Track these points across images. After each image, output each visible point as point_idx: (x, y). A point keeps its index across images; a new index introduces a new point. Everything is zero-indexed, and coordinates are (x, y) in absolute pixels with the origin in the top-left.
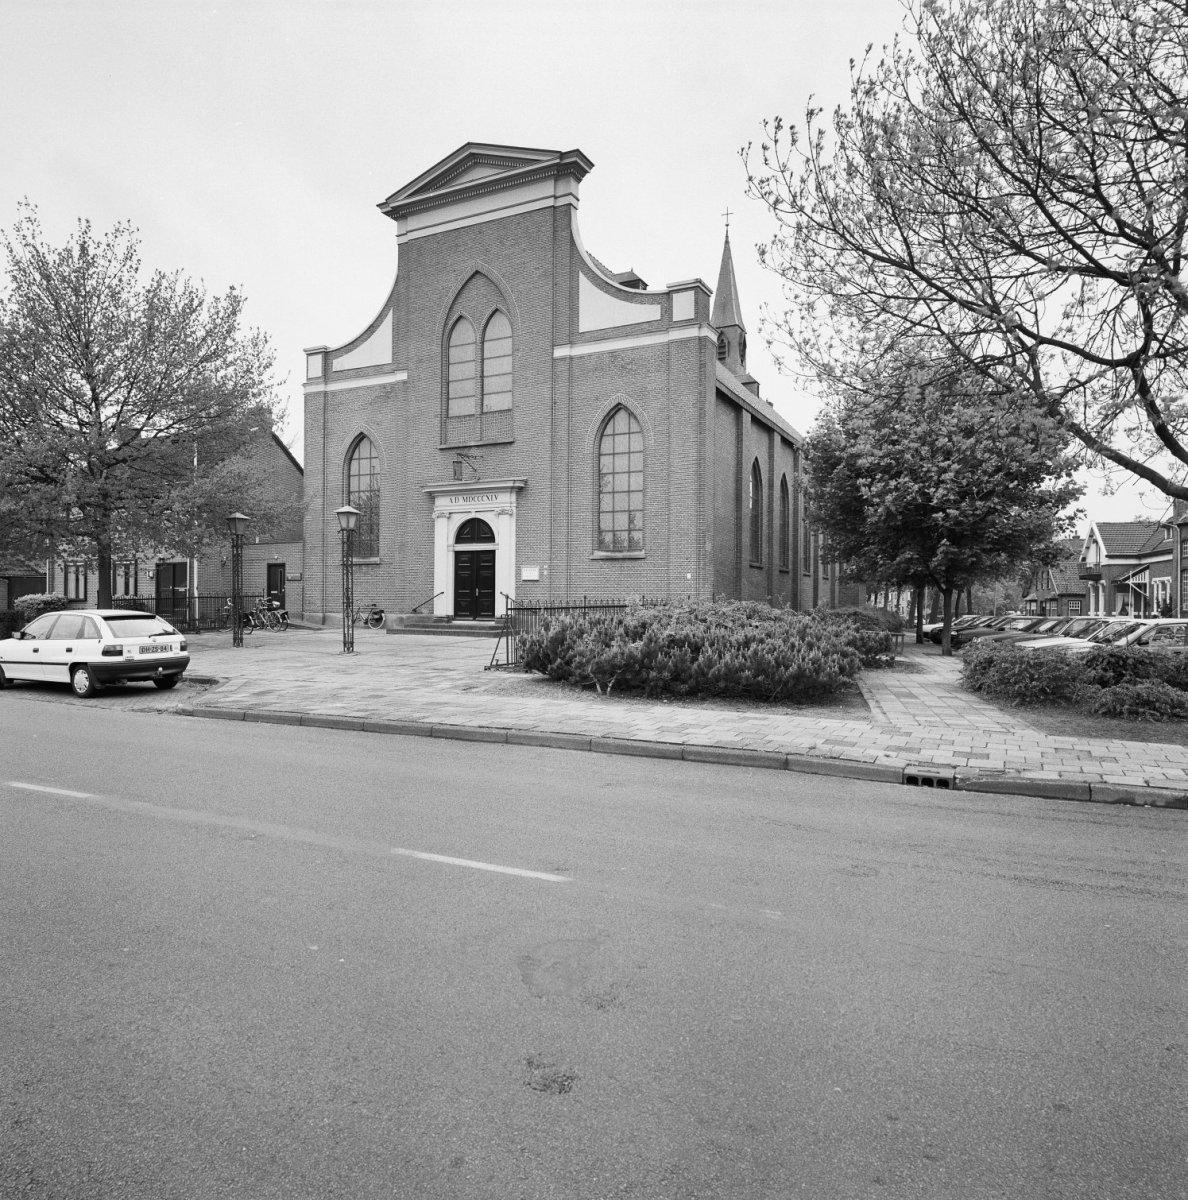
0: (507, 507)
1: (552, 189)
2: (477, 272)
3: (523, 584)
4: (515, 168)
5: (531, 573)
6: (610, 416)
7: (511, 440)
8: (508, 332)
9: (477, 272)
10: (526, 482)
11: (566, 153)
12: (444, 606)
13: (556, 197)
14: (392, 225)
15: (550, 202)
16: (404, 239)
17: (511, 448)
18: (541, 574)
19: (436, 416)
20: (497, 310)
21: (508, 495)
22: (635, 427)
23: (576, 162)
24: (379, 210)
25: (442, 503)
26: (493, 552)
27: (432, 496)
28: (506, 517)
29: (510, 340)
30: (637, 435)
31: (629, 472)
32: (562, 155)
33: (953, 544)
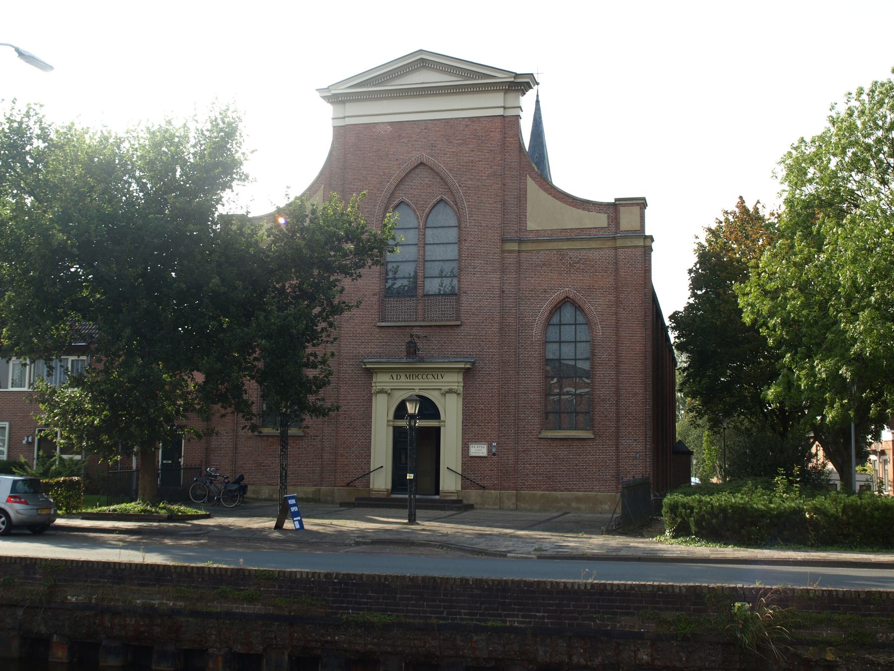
0: (454, 387)
1: (502, 101)
2: (422, 163)
3: (468, 461)
4: (473, 79)
5: (479, 450)
6: (557, 308)
7: (458, 323)
8: (453, 222)
9: (422, 163)
10: (473, 363)
11: (519, 74)
12: (381, 481)
13: (505, 108)
14: (328, 110)
15: (500, 112)
16: (341, 123)
17: (457, 330)
18: (489, 451)
19: (375, 294)
20: (441, 200)
21: (455, 375)
22: (580, 319)
23: (529, 82)
24: (318, 94)
25: (381, 381)
26: (438, 429)
27: (370, 373)
28: (455, 396)
29: (427, 258)
30: (583, 327)
31: (575, 342)
32: (517, 75)
33: (781, 324)
